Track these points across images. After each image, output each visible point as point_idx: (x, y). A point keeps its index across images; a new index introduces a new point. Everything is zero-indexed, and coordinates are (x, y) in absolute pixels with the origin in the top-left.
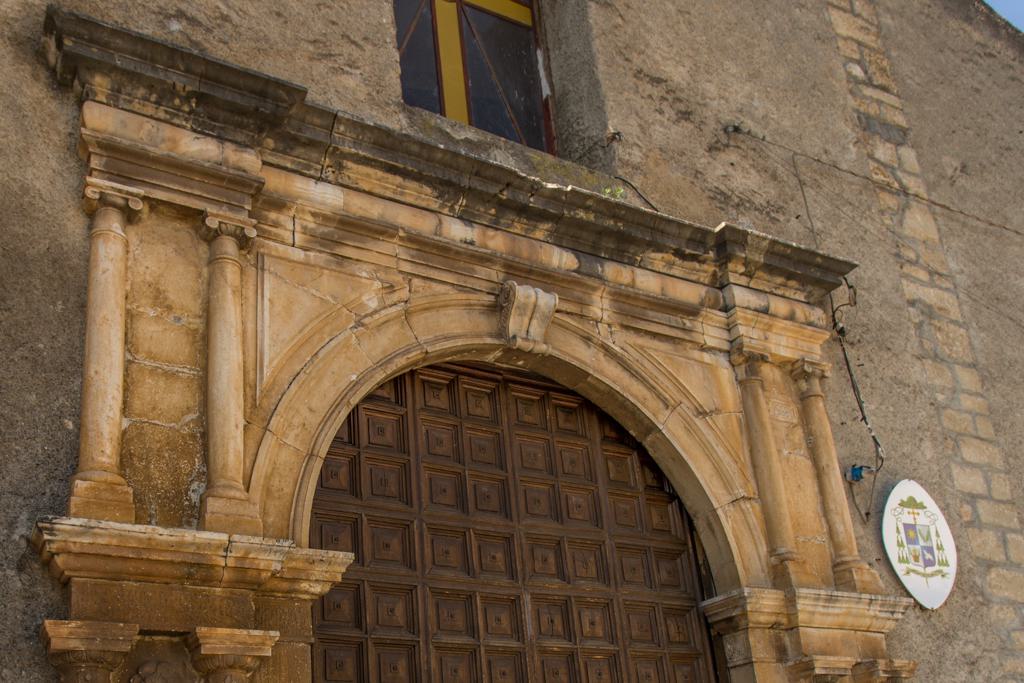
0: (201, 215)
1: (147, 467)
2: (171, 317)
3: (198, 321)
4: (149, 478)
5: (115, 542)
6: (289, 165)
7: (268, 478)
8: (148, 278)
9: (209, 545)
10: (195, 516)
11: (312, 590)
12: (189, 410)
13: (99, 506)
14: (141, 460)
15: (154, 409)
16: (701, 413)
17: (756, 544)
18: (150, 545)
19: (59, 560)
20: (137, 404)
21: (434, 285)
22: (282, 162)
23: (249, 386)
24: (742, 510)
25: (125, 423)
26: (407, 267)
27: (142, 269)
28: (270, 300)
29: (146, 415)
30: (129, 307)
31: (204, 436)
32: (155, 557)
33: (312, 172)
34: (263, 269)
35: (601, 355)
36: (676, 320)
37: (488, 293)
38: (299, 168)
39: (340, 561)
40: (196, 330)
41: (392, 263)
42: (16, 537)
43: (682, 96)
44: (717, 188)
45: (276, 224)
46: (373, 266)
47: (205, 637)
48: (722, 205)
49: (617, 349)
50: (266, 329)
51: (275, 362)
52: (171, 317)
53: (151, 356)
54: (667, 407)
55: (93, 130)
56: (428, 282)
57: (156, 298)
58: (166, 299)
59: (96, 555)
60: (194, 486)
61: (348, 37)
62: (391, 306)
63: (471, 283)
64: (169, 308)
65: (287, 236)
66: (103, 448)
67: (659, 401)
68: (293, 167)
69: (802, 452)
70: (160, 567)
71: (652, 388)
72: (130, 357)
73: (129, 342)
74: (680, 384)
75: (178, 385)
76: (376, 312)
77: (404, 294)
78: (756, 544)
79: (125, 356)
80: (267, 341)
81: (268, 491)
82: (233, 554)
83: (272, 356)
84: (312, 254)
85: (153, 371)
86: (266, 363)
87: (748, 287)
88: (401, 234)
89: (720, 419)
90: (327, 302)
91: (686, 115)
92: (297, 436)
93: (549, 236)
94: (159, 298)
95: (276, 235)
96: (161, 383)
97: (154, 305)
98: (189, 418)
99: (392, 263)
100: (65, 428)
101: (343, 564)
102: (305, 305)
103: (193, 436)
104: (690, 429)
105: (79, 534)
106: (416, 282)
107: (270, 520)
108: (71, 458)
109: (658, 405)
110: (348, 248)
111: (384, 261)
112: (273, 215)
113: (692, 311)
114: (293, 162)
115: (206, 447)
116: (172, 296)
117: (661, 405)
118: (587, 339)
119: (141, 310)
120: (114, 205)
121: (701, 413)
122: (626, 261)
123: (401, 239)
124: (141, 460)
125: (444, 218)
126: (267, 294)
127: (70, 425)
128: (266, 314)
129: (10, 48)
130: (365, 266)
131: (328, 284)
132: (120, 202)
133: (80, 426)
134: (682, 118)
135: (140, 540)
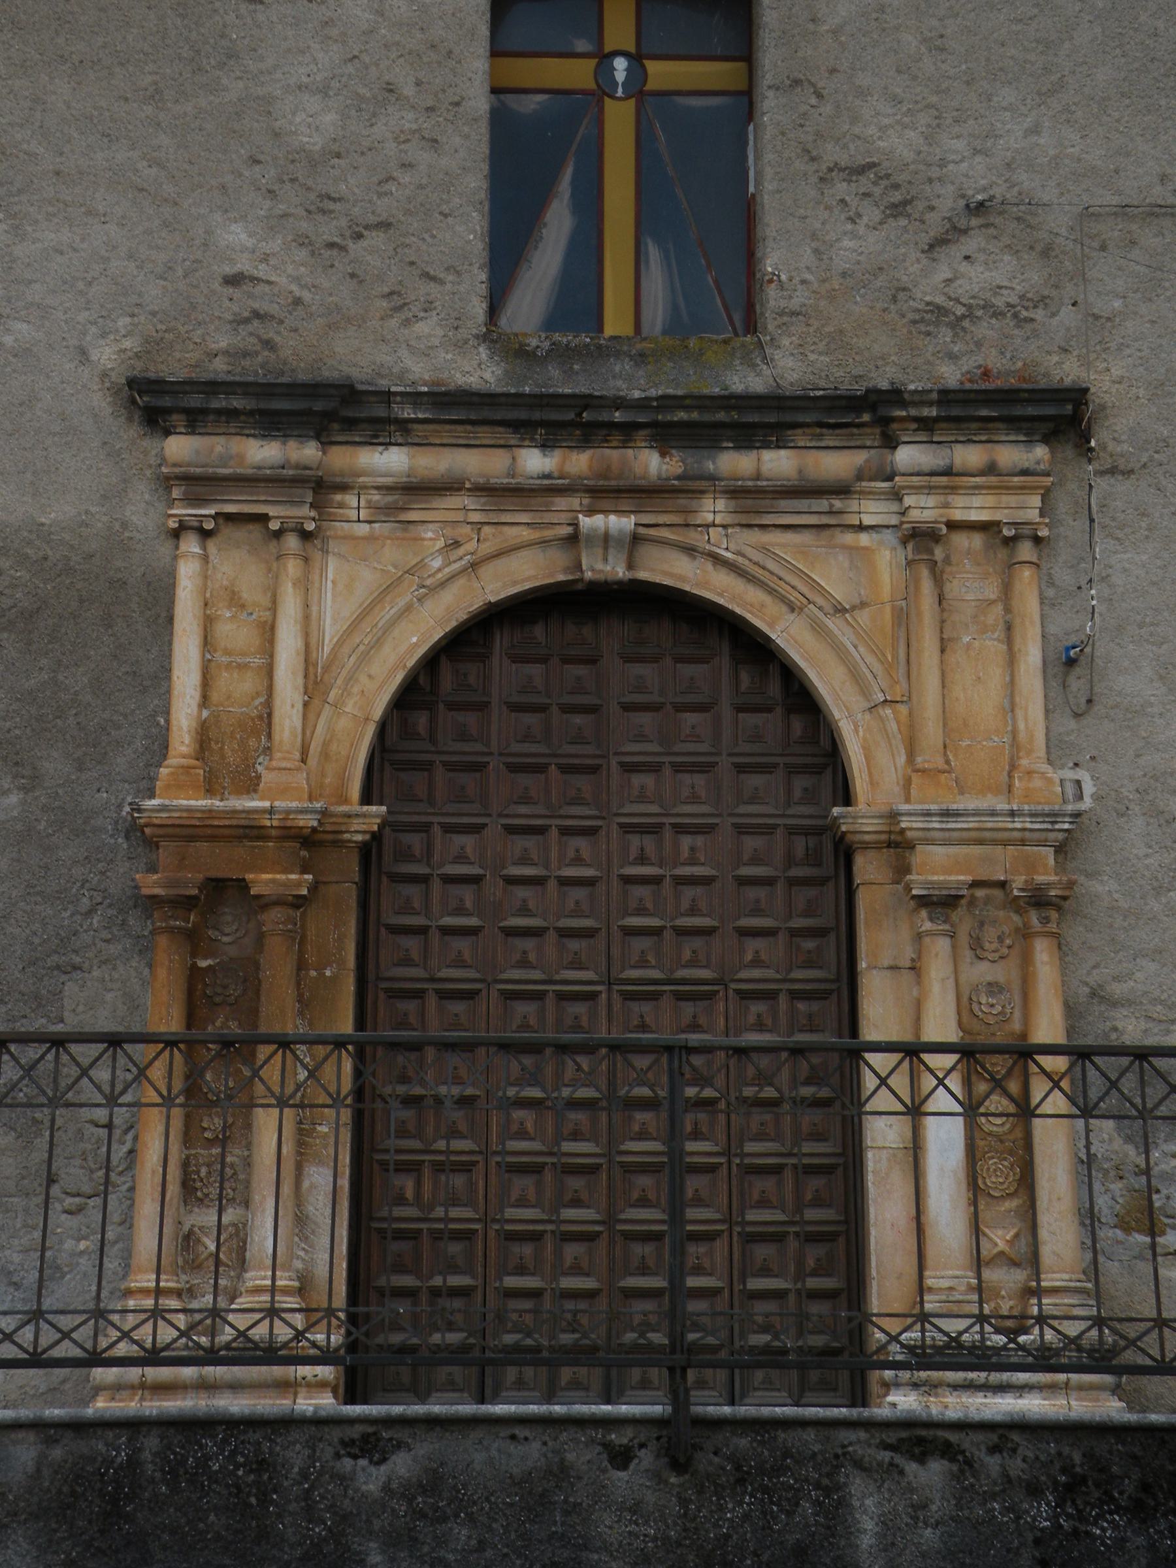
0: (263, 518)
1: (222, 749)
2: (245, 614)
3: (268, 613)
4: (223, 757)
5: (185, 815)
6: (357, 439)
7: (326, 744)
8: (225, 583)
9: (255, 811)
10: (251, 786)
11: (354, 839)
12: (258, 694)
13: (176, 786)
14: (217, 743)
15: (229, 697)
16: (840, 610)
17: (893, 755)
18: (210, 813)
19: (147, 830)
20: (215, 696)
21: (506, 529)
22: (350, 439)
23: (308, 661)
24: (880, 717)
25: (205, 713)
26: (476, 517)
27: (219, 576)
28: (333, 582)
29: (222, 705)
30: (208, 612)
31: (267, 717)
32: (216, 823)
33: (381, 440)
34: (327, 552)
35: (709, 566)
36: (823, 504)
37: (569, 524)
38: (368, 440)
39: (378, 809)
40: (266, 622)
41: (460, 516)
42: (124, 813)
43: (901, 178)
44: (928, 304)
45: (341, 506)
46: (437, 525)
47: (252, 882)
48: (931, 328)
49: (728, 555)
50: (329, 609)
51: (335, 640)
52: (245, 614)
53: (227, 652)
54: (793, 610)
55: (175, 465)
56: (500, 527)
57: (232, 599)
58: (240, 598)
59: (173, 826)
60: (260, 760)
61: (428, 273)
62: (455, 562)
63: (548, 518)
64: (243, 606)
65: (353, 515)
66: (182, 739)
67: (782, 605)
68: (362, 440)
69: (996, 635)
70: (221, 830)
71: (771, 591)
72: (208, 656)
73: (207, 642)
74: (814, 580)
75: (249, 674)
76: (439, 570)
77: (471, 546)
78: (893, 755)
79: (204, 655)
80: (328, 621)
81: (325, 755)
82: (277, 817)
83: (330, 631)
84: (377, 525)
85: (228, 667)
86: (326, 642)
87: (932, 442)
88: (468, 485)
89: (864, 617)
90: (389, 572)
91: (898, 209)
92: (356, 703)
93: (651, 441)
94: (234, 600)
95: (342, 515)
96: (235, 675)
97: (229, 607)
98: (257, 702)
99: (460, 516)
100: (158, 724)
101: (377, 816)
102: (367, 579)
103: (260, 717)
104: (819, 629)
105: (159, 811)
106: (487, 530)
107: (327, 781)
108: (161, 746)
109: (773, 607)
110: (412, 512)
111: (451, 516)
112: (338, 497)
113: (842, 490)
114: (361, 436)
115: (270, 725)
116: (245, 595)
117: (784, 609)
118: (690, 551)
119: (219, 613)
120: (192, 528)
121: (840, 610)
122: (758, 445)
123: (469, 490)
124: (217, 743)
125: (517, 451)
126: (330, 576)
127: (162, 721)
128: (329, 595)
129: (109, 399)
130: (431, 526)
131: (392, 555)
132: (196, 524)
133: (168, 721)
134: (888, 217)
135: (203, 812)
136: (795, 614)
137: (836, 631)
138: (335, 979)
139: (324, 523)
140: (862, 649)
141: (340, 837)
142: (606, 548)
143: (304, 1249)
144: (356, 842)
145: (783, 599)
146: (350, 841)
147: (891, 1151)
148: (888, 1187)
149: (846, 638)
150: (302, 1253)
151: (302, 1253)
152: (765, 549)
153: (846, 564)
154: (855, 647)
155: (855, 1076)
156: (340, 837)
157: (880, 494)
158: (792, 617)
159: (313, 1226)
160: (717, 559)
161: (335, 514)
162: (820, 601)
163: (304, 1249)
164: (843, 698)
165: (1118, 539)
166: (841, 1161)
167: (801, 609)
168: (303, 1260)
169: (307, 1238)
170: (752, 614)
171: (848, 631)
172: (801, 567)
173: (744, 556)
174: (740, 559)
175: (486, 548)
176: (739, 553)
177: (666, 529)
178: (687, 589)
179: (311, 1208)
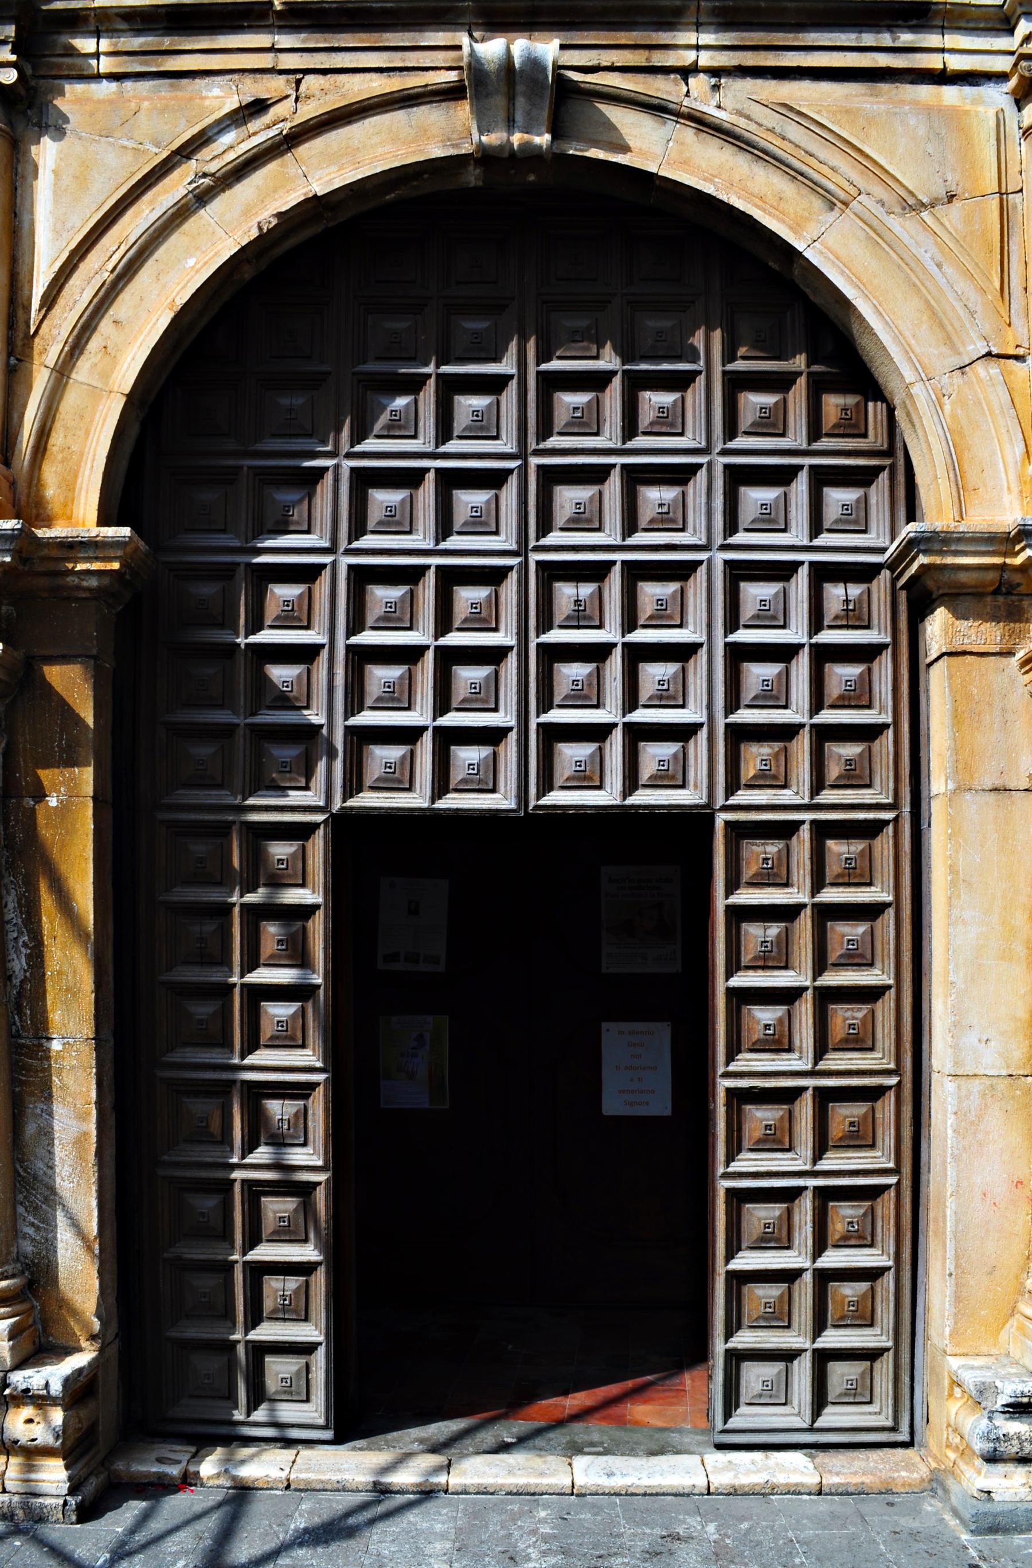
11: (85, 584)
16: (912, 206)
71: (797, 175)
74: (867, 157)
89: (953, 215)
95: (70, 67)
117: (817, 203)
121: (912, 206)
136: (836, 212)
137: (906, 239)
138: (64, 809)
139: (42, 81)
140: (948, 269)
141: (60, 581)
142: (511, 98)
143: (32, 1224)
144: (89, 589)
145: (815, 187)
146: (79, 588)
147: (987, 1082)
148: (980, 1136)
149: (926, 252)
150: (31, 1231)
151: (31, 1231)
152: (787, 109)
153: (922, 131)
154: (939, 266)
155: (348, 765)
156: (60, 581)
157: (977, 20)
158: (831, 216)
159: (44, 1191)
160: (701, 122)
161: (59, 66)
162: (879, 191)
163: (32, 1224)
164: (918, 350)
165: (616, 1554)
166: (893, 1081)
167: (846, 204)
168: (33, 1240)
169: (36, 1208)
170: (764, 210)
171: (922, 237)
172: (845, 135)
173: (748, 118)
174: (742, 122)
175: (309, 111)
176: (740, 113)
177: (616, 74)
178: (653, 169)
179: (40, 1165)
